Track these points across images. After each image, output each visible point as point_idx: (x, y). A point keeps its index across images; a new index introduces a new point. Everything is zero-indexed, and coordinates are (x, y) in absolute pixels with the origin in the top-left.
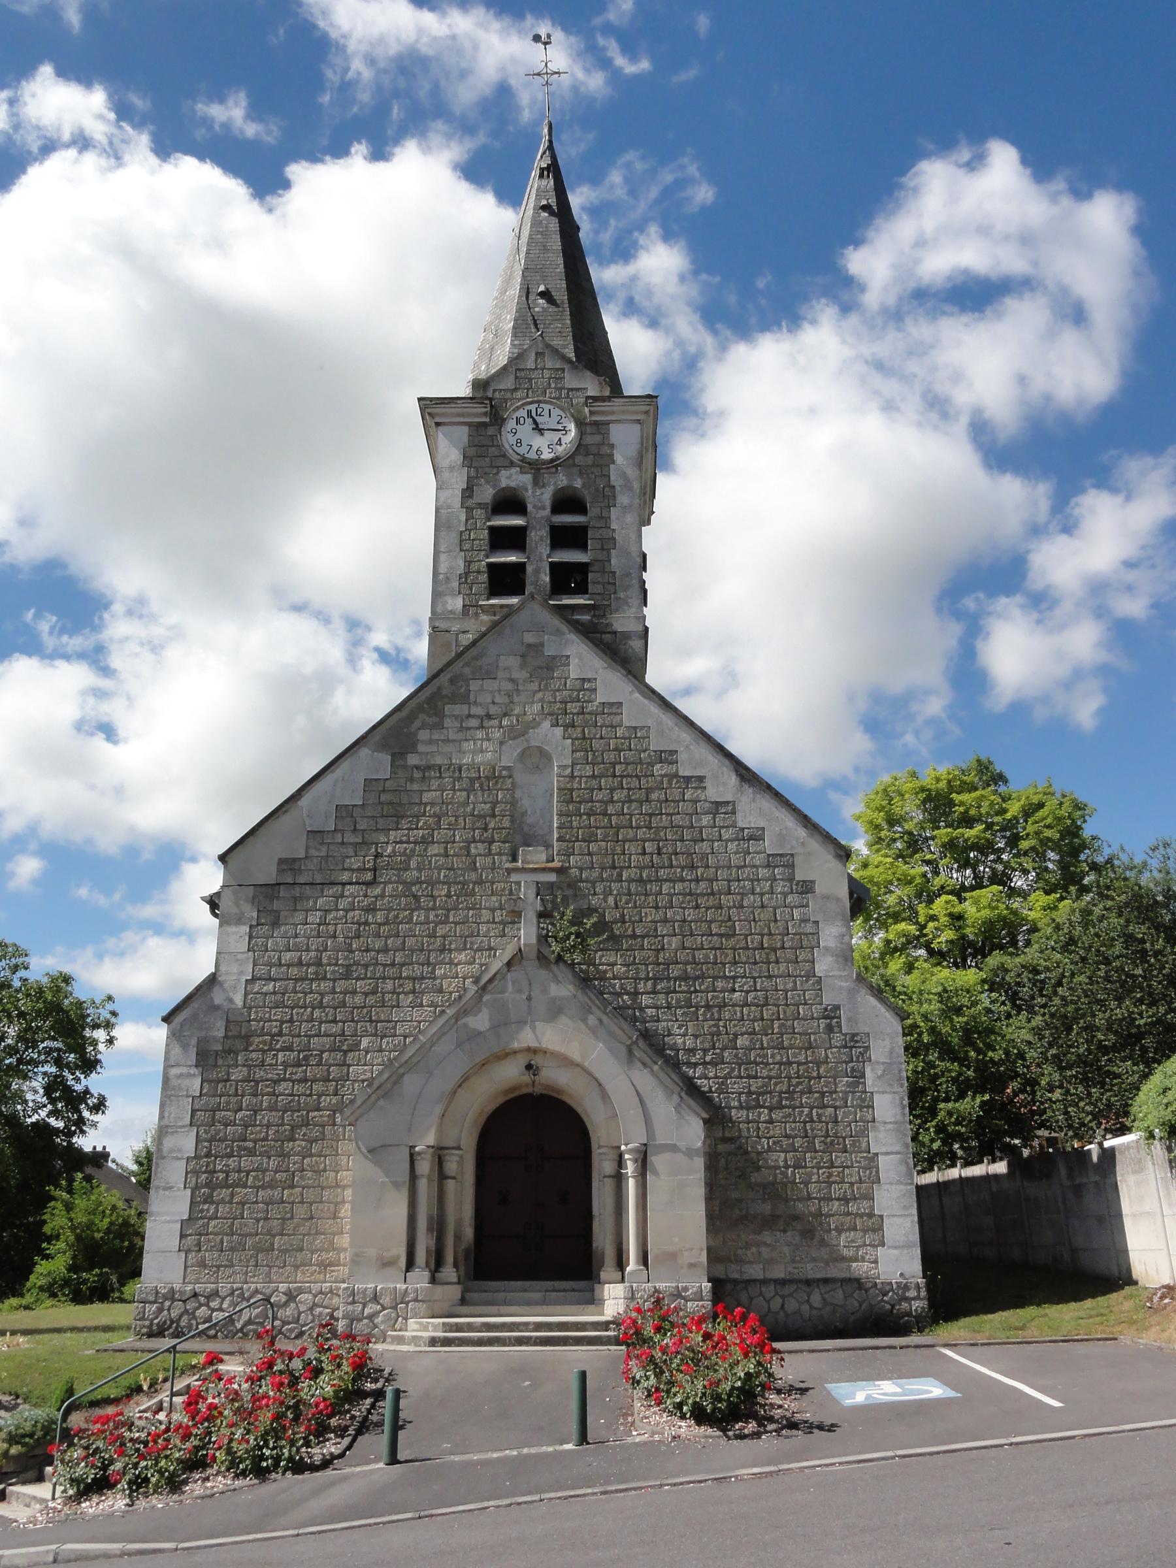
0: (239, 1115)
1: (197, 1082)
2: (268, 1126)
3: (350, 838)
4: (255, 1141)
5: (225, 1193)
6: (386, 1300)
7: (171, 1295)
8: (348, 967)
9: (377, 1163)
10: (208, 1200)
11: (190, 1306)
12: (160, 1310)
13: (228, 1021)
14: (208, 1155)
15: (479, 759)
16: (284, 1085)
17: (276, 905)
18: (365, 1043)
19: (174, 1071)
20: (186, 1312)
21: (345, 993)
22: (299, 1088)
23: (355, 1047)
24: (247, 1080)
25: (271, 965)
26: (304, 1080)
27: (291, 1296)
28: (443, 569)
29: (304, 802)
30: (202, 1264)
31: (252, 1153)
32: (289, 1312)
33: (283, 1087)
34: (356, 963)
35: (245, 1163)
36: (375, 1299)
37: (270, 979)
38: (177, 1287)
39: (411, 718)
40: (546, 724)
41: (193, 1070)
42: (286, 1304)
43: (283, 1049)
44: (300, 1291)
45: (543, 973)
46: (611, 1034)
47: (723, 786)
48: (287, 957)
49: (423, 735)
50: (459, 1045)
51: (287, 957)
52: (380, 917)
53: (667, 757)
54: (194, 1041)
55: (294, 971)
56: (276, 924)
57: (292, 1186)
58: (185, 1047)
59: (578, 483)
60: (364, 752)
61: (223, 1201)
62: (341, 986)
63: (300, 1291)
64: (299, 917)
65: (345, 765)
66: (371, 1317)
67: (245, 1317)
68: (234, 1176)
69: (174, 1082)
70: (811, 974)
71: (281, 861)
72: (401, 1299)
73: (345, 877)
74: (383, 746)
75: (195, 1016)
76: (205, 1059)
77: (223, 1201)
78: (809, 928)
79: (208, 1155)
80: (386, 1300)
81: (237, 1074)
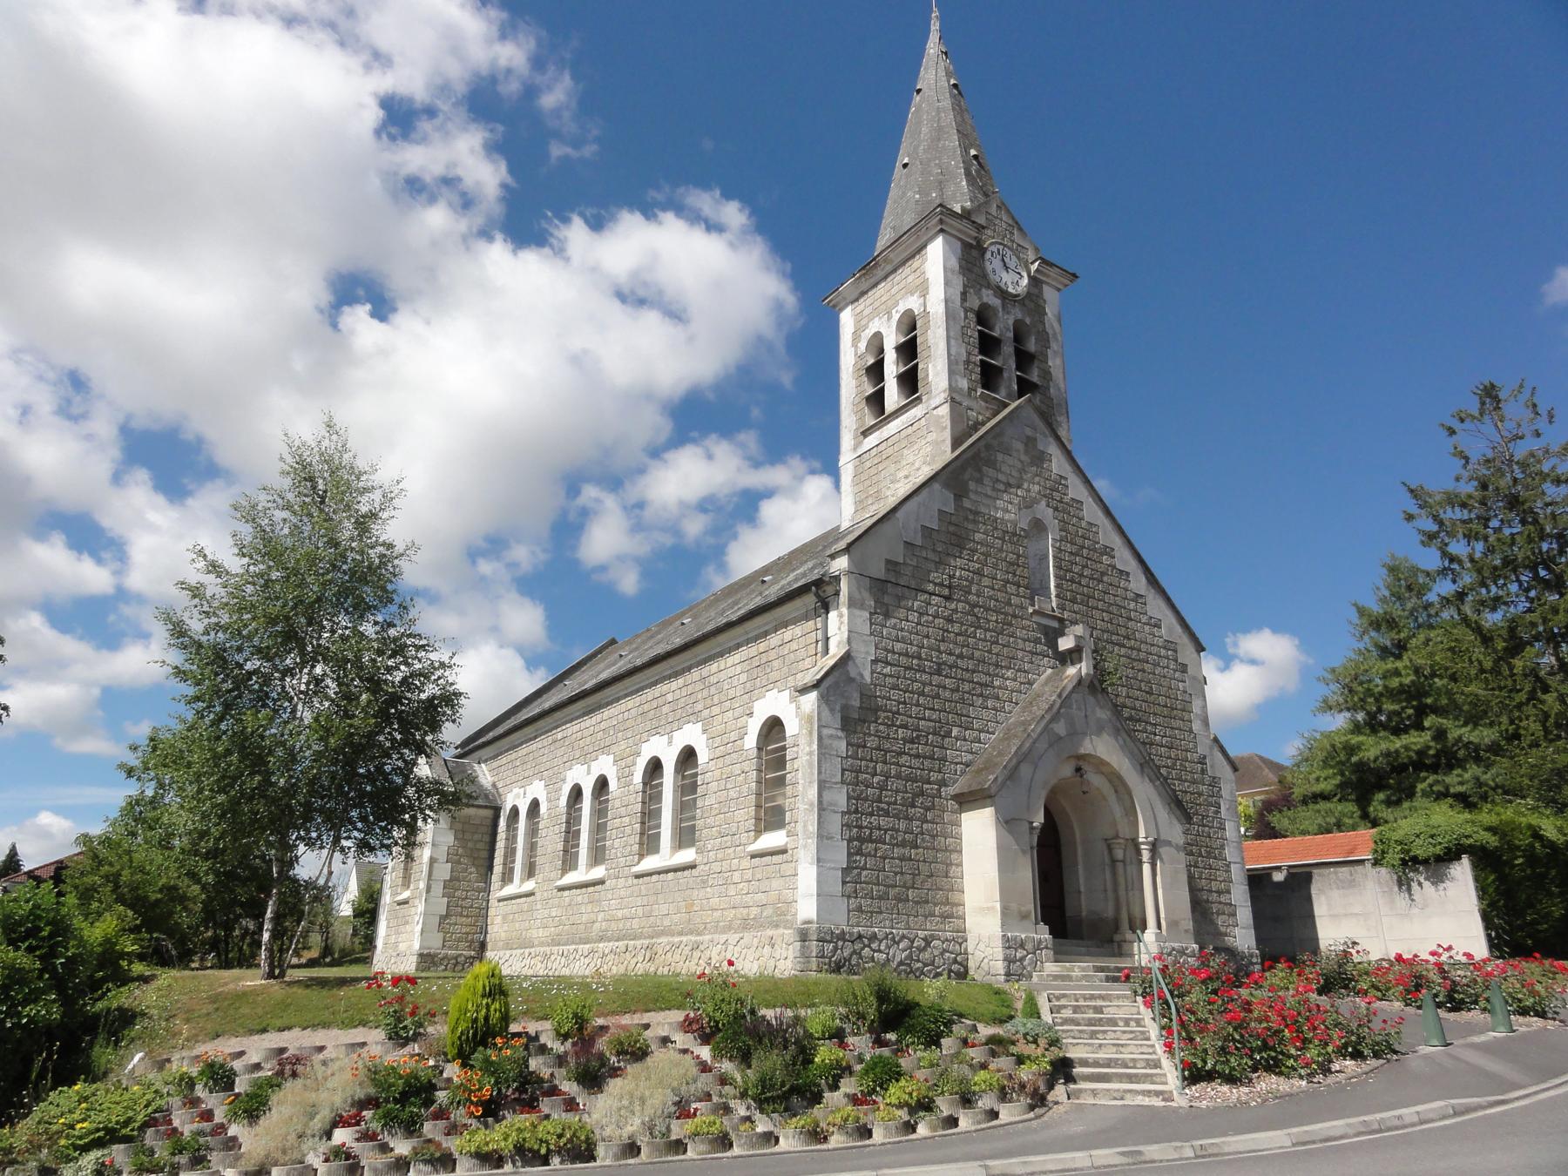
0: (876, 779)
1: (843, 744)
2: (897, 791)
3: (931, 555)
4: (889, 804)
5: (871, 846)
6: (1029, 946)
7: (842, 936)
8: (939, 664)
9: (1011, 832)
10: (859, 852)
11: (858, 946)
12: (836, 949)
13: (862, 695)
14: (856, 811)
15: (1007, 517)
16: (905, 758)
17: (887, 599)
18: (955, 732)
19: (826, 732)
20: (854, 952)
21: (938, 686)
22: (915, 763)
23: (948, 734)
24: (878, 749)
25: (888, 651)
26: (917, 756)
27: (928, 941)
28: (953, 352)
29: (899, 514)
30: (859, 909)
31: (887, 814)
32: (926, 956)
33: (904, 759)
34: (944, 663)
35: (883, 821)
36: (1022, 946)
37: (888, 663)
38: (847, 929)
39: (963, 468)
40: (1043, 503)
41: (840, 733)
42: (924, 949)
43: (901, 726)
44: (933, 938)
45: (1091, 699)
46: (1132, 753)
47: (1138, 583)
48: (898, 646)
49: (972, 486)
50: (1051, 745)
51: (898, 646)
52: (956, 628)
53: (1108, 551)
54: (838, 707)
55: (903, 660)
56: (887, 615)
57: (917, 847)
58: (832, 710)
59: (1028, 321)
60: (936, 486)
61: (869, 855)
62: (936, 679)
63: (933, 938)
64: (902, 613)
65: (925, 493)
66: (1022, 959)
67: (898, 959)
68: (876, 833)
69: (827, 741)
70: (1191, 731)
71: (888, 562)
72: (1038, 947)
73: (931, 587)
74: (947, 485)
75: (836, 684)
76: (848, 725)
77: (869, 855)
78: (1187, 698)
79: (856, 811)
80: (1029, 946)
81: (872, 742)
